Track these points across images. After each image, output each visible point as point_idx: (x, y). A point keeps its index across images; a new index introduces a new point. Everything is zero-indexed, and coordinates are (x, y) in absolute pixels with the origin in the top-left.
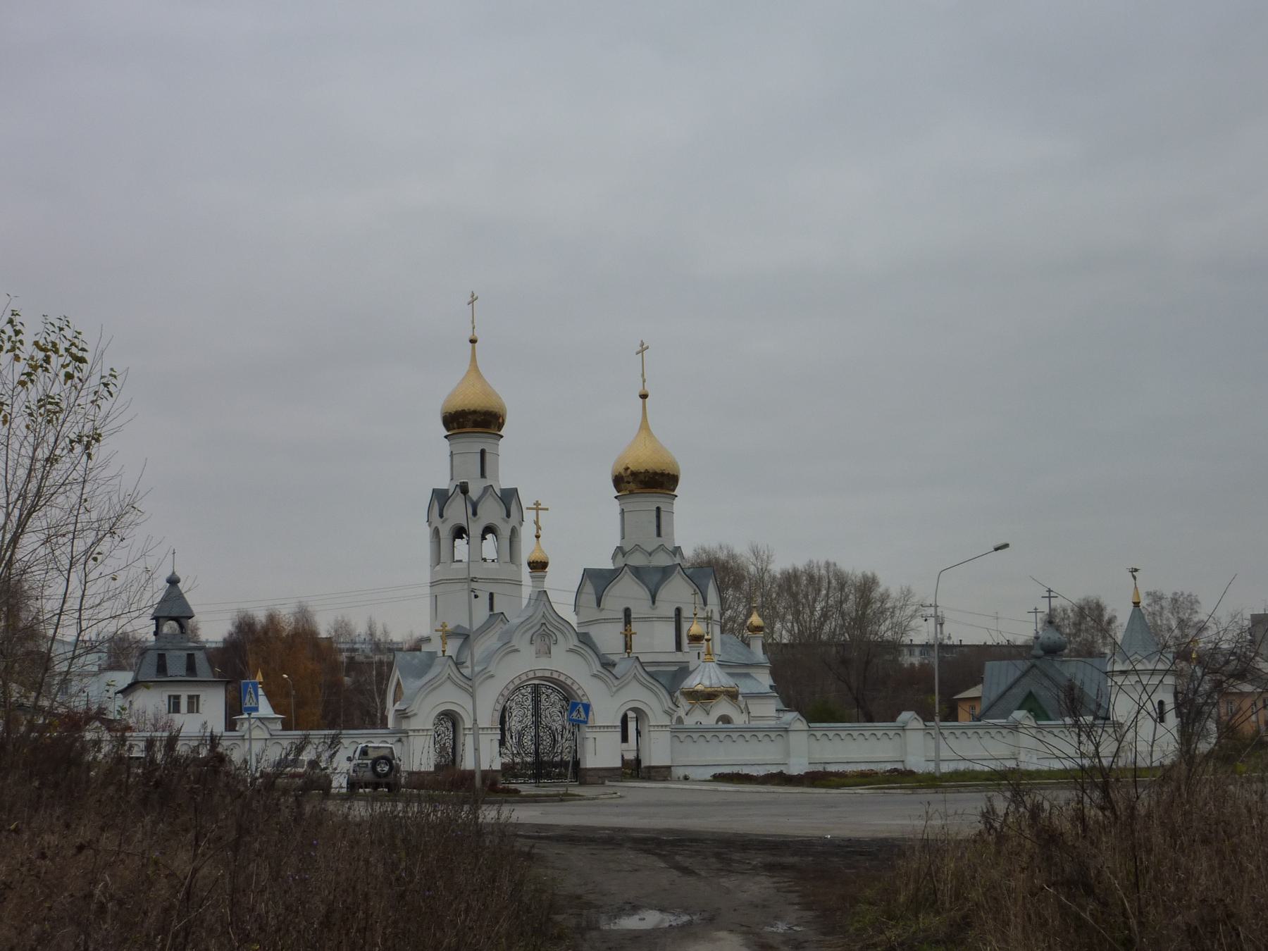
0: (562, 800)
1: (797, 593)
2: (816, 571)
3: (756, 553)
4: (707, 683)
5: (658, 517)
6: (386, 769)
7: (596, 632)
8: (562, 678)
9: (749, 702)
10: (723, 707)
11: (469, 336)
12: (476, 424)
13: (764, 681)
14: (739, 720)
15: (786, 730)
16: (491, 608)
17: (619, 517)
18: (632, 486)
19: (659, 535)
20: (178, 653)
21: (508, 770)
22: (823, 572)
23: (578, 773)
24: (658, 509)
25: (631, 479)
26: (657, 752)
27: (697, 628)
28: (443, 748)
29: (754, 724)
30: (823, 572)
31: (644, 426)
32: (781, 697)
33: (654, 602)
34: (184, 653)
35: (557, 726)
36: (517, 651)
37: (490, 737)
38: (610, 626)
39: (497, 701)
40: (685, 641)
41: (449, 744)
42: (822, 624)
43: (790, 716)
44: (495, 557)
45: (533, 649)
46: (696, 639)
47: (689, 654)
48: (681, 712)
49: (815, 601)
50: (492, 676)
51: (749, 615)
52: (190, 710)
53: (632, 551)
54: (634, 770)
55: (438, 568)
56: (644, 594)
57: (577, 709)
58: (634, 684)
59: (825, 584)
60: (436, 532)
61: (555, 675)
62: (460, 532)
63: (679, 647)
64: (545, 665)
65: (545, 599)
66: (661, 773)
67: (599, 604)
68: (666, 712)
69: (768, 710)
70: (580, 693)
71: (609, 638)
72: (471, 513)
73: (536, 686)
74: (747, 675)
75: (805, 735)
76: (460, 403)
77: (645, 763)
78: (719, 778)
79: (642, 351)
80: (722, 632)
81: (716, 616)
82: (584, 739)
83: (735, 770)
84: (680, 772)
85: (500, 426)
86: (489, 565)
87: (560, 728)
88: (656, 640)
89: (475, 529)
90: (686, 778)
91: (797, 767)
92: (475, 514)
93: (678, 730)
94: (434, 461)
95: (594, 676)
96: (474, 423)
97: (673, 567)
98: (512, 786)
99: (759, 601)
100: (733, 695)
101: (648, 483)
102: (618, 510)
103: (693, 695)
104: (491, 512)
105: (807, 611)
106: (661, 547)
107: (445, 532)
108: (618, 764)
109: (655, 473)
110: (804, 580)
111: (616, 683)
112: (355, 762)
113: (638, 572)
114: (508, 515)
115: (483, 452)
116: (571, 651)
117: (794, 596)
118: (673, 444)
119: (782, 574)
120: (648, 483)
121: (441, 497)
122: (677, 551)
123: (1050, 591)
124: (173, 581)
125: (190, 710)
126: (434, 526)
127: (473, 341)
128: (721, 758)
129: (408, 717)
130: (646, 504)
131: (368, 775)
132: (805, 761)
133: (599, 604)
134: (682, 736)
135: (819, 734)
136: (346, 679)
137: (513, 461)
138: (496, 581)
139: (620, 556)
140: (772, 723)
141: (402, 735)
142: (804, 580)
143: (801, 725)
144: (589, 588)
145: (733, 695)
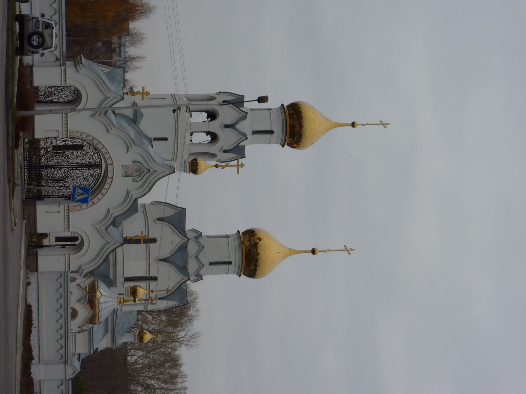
0: (9, 180)
1: (164, 367)
2: (180, 380)
3: (194, 336)
4: (102, 300)
5: (224, 263)
6: (35, 43)
7: (139, 217)
8: (107, 186)
9: (87, 332)
10: (83, 313)
12: (292, 127)
13: (102, 343)
14: (74, 325)
15: (66, 362)
16: (156, 139)
17: (223, 233)
18: (247, 243)
19: (211, 264)
21: (34, 145)
22: (179, 385)
23: (33, 198)
24: (230, 263)
25: (253, 242)
26: (50, 261)
27: (142, 293)
28: (51, 94)
29: (70, 336)
30: (179, 385)
31: (292, 252)
32: (90, 356)
33: (161, 260)
35: (70, 182)
36: (128, 150)
37: (60, 131)
39: (88, 136)
40: (132, 284)
41: (55, 98)
42: (142, 385)
43: (77, 365)
44: (194, 142)
45: (130, 163)
46: (134, 292)
47: (123, 287)
48: (80, 280)
49: (159, 379)
50: (108, 131)
51: (151, 332)
53: (199, 244)
54: (35, 242)
55: (185, 99)
56: (166, 252)
57: (86, 195)
58: (102, 243)
59: (171, 387)
60: (212, 98)
61: (109, 180)
62: (212, 116)
63: (128, 279)
64: (117, 172)
65: (167, 172)
66: (32, 265)
67: (159, 219)
68: (80, 267)
69: (81, 347)
70: (95, 200)
71: (134, 227)
72: (226, 126)
73: (99, 166)
74: (106, 331)
75: (62, 377)
76: (308, 116)
77: (40, 251)
78: (28, 309)
79: (346, 249)
80: (139, 312)
81: (150, 307)
82: (59, 204)
83: (35, 322)
84: (33, 279)
85: (291, 145)
86: (188, 137)
87: (67, 184)
88: (133, 262)
89: (215, 126)
90: (28, 284)
91: (38, 371)
92: (226, 126)
93: (66, 277)
95: (109, 211)
96: (294, 126)
97: (187, 275)
98: (21, 143)
99: (159, 339)
100: (92, 320)
101: (249, 255)
102: (229, 233)
103: (92, 290)
104: (228, 139)
105: (151, 374)
106: (202, 266)
107: (213, 105)
108: (36, 137)
109: (257, 260)
110: (173, 371)
111: (103, 228)
112: (41, 19)
113: (183, 248)
114: (225, 151)
115: (271, 132)
116: (128, 192)
117: (162, 365)
118: (279, 275)
119: (178, 356)
120: (249, 255)
122: (199, 277)
126: (216, 96)
128: (43, 301)
129: (75, 66)
130: (234, 254)
131: (30, 27)
132: (42, 377)
133: (159, 219)
134: (61, 280)
135: (63, 387)
136: (100, 44)
137: (267, 155)
139: (195, 235)
140: (71, 351)
141: (60, 61)
142: (173, 371)
143: (70, 374)
144: (169, 212)
145: (92, 320)
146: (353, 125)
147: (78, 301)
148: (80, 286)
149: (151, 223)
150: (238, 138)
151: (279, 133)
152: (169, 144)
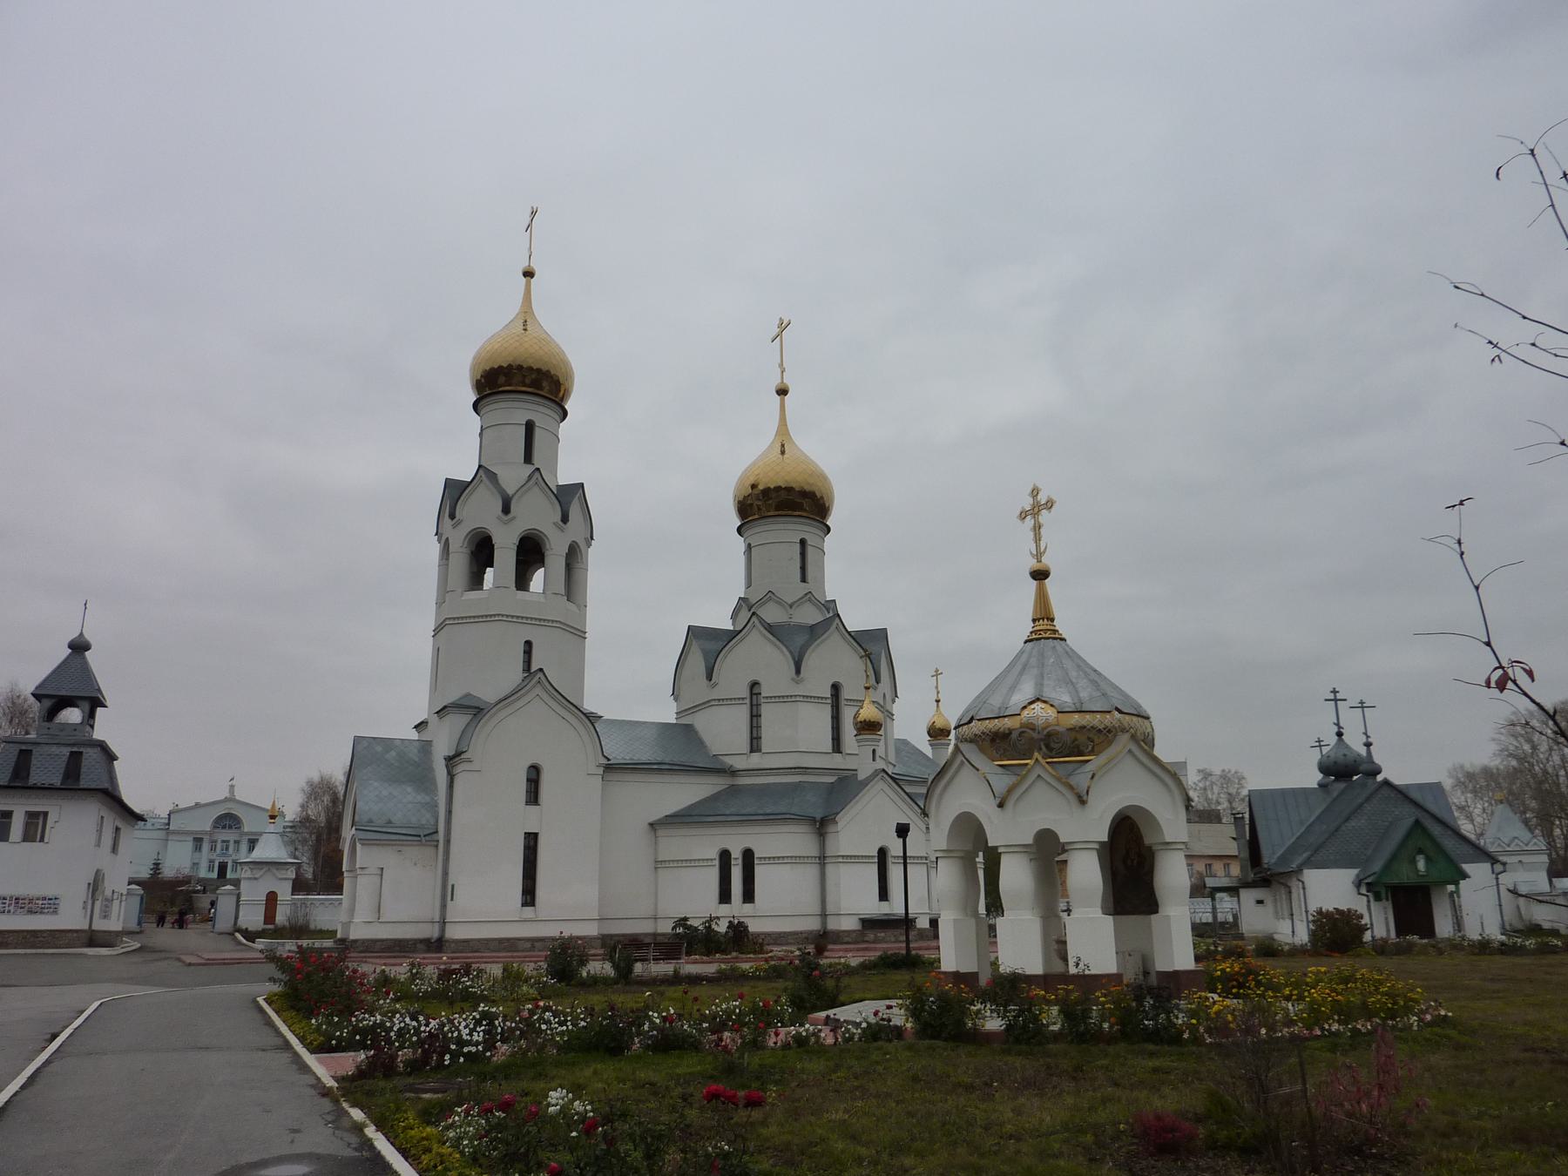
5: (803, 554)
11: (523, 265)
17: (742, 559)
19: (804, 580)
20: (54, 749)
33: (798, 672)
34: (66, 751)
38: (723, 712)
40: (848, 730)
52: (28, 836)
53: (762, 602)
63: (837, 745)
67: (709, 677)
92: (506, 509)
94: (457, 443)
102: (743, 548)
114: (565, 519)
118: (824, 453)
121: (455, 491)
123: (1334, 692)
124: (79, 647)
125: (28, 836)
127: (529, 274)
130: (784, 533)
133: (709, 677)
137: (580, 449)
138: (540, 622)
144: (697, 663)
146: (529, 274)
147: (1082, 802)
148: (1010, 791)
149: (716, 694)
150: (536, 489)
151: (540, 413)
152: (537, 636)
